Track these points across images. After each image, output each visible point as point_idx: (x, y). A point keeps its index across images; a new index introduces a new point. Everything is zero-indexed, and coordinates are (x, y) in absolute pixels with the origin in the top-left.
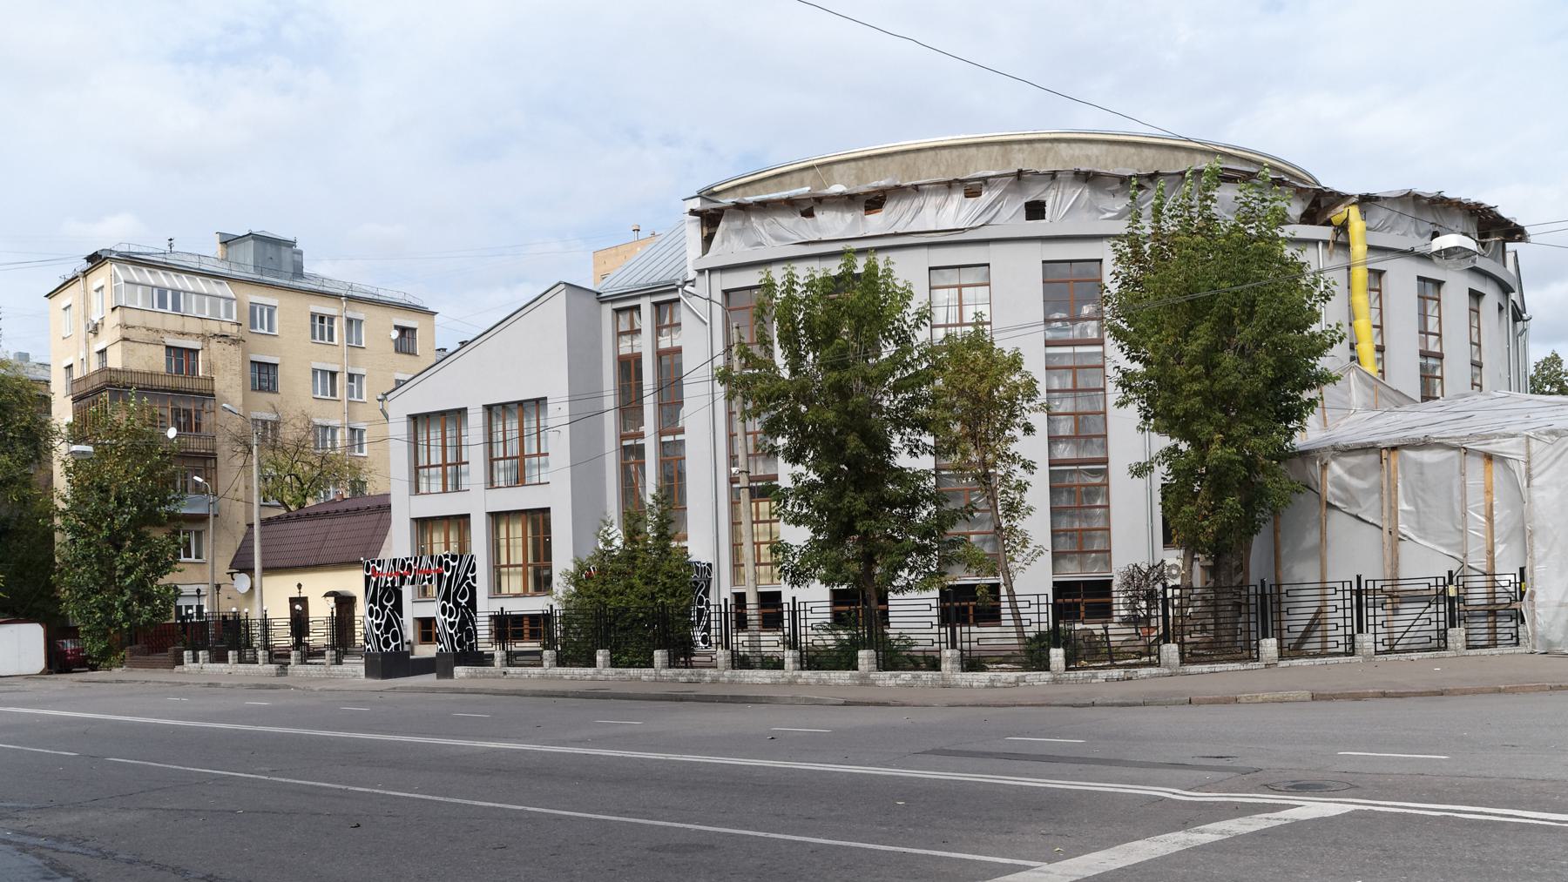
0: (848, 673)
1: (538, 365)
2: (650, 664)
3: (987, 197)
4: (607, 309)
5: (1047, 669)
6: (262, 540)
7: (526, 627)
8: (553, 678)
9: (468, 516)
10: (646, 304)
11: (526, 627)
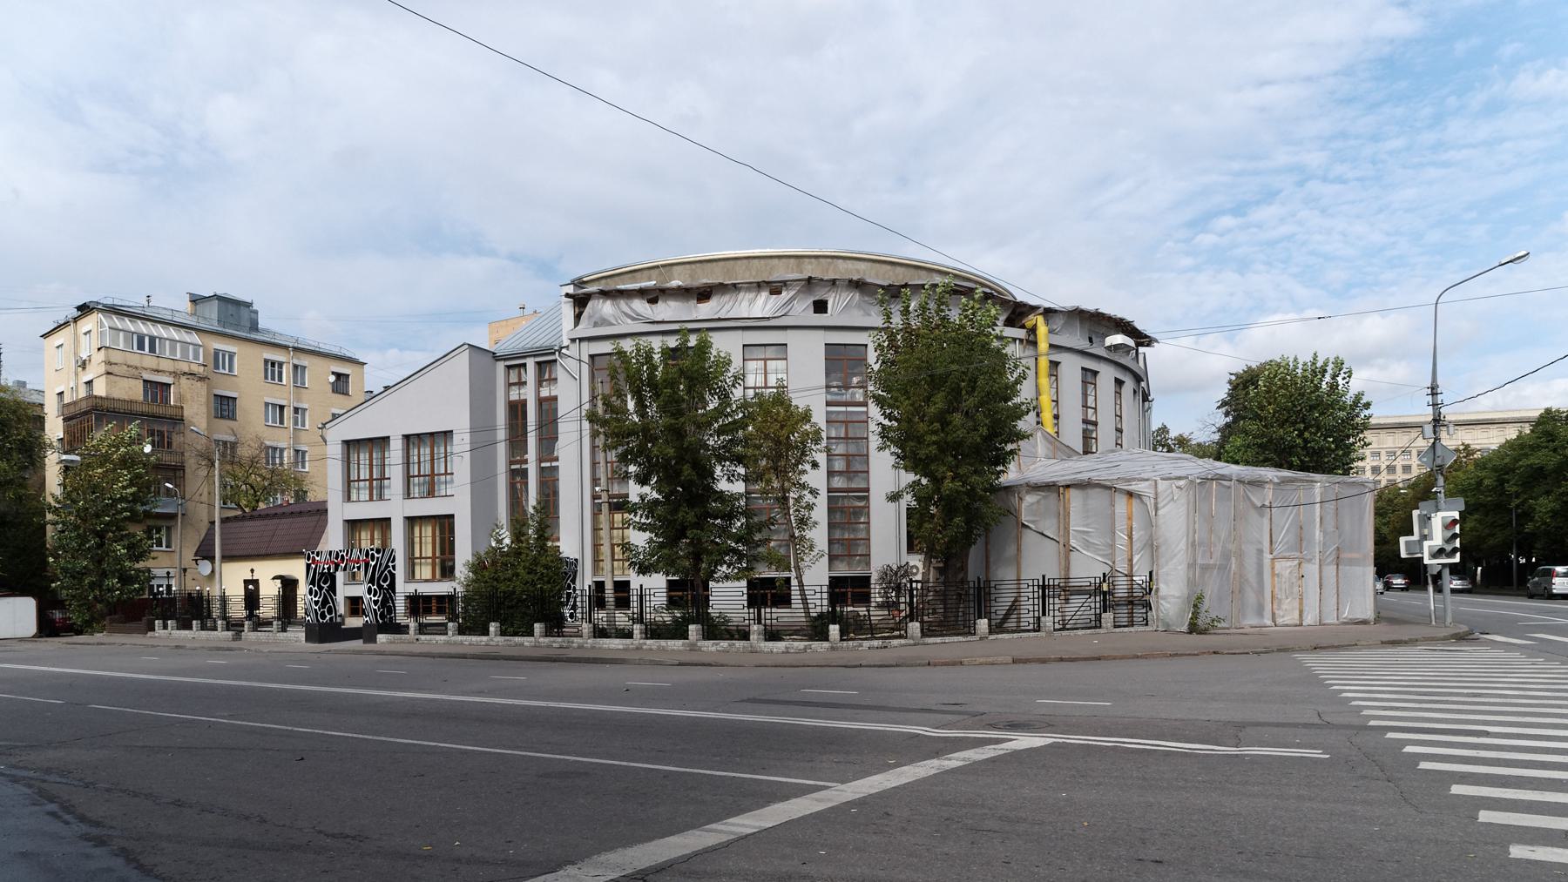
0: (681, 642)
1: (446, 405)
2: (531, 634)
3: (786, 295)
4: (501, 366)
5: (827, 639)
6: (222, 534)
7: (434, 605)
8: (455, 643)
9: (389, 519)
10: (530, 363)
11: (434, 605)
